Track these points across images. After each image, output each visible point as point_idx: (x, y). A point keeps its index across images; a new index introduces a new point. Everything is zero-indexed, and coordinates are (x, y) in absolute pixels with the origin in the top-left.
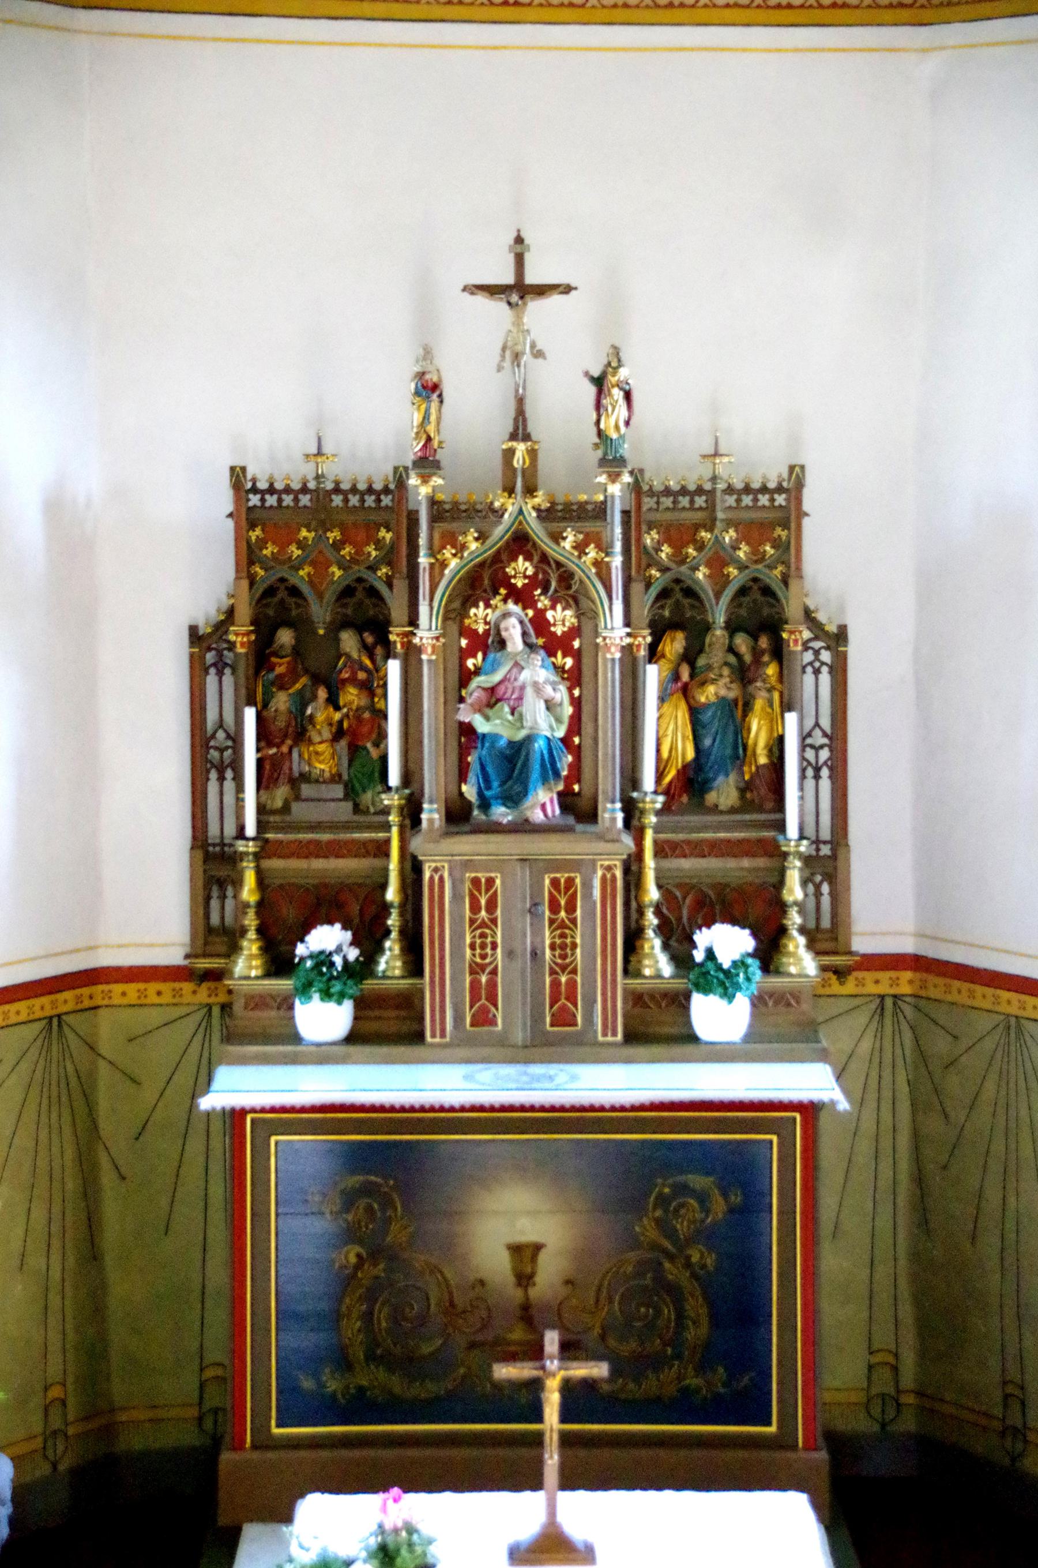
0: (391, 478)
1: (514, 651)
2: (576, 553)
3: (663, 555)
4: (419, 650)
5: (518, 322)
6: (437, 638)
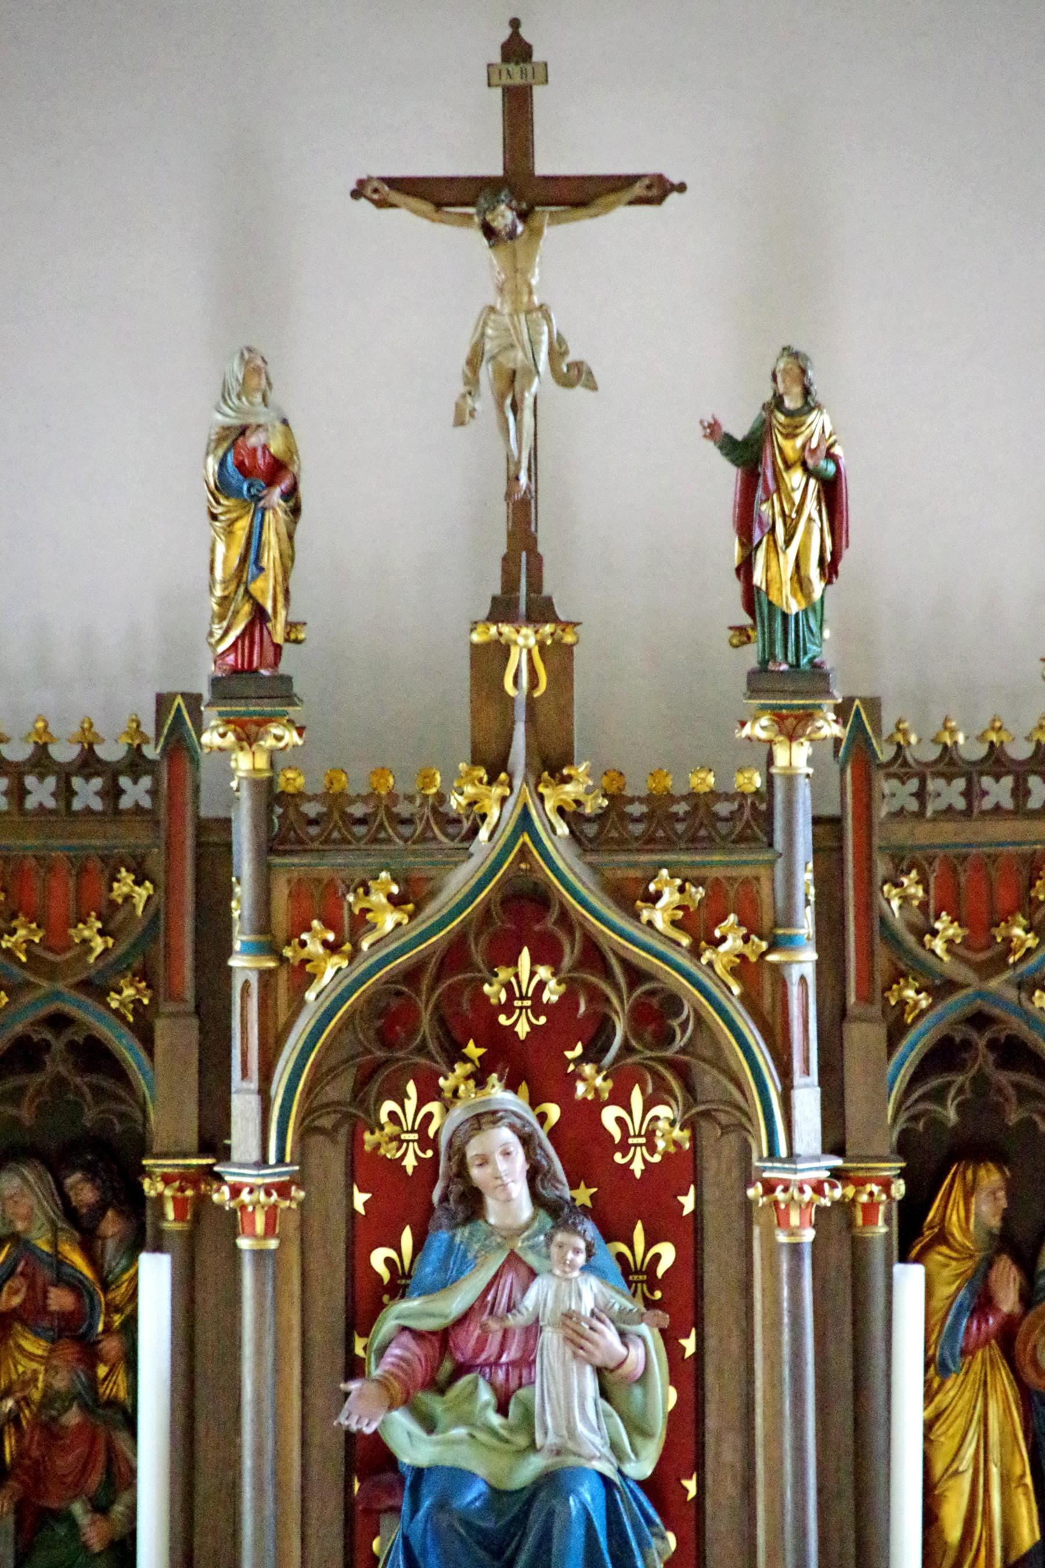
0: (149, 728)
1: (509, 1221)
2: (685, 941)
3: (939, 945)
4: (231, 1223)
5: (514, 283)
6: (283, 1190)
